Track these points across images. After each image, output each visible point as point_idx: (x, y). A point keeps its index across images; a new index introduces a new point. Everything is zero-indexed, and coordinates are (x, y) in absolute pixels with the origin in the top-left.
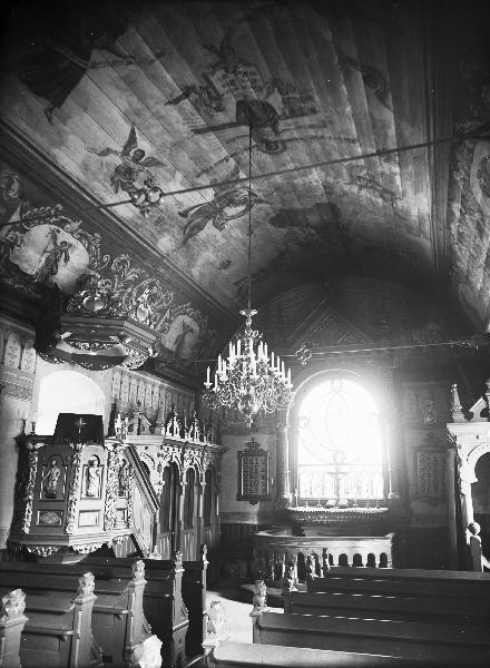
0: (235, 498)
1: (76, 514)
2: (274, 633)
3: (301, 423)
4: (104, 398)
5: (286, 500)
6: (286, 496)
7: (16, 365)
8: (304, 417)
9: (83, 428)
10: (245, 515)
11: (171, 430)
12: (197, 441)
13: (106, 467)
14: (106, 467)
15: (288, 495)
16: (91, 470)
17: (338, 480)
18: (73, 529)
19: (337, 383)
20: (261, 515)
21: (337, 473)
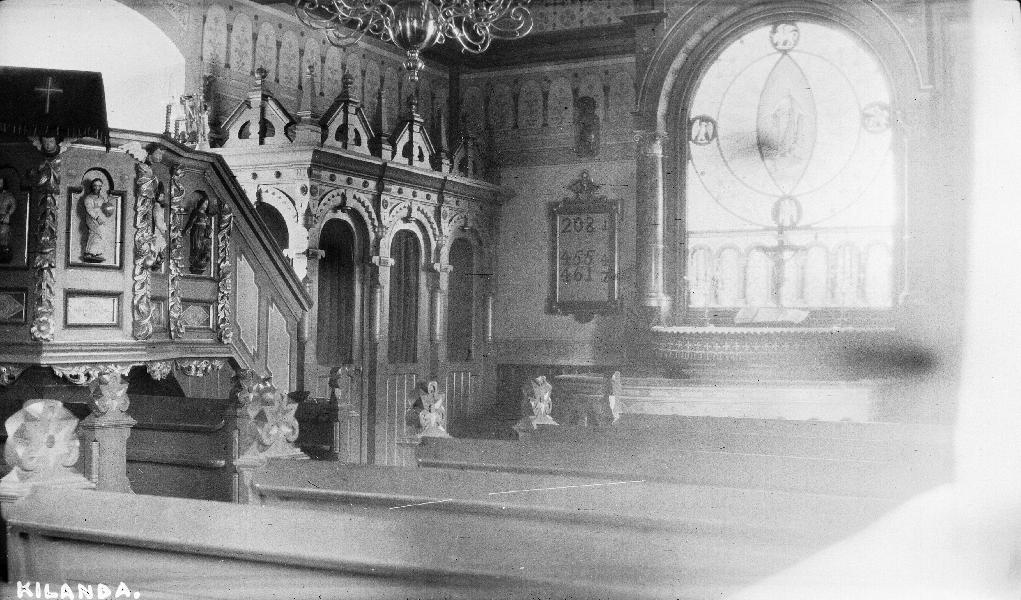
0: (542, 306)
1: (57, 301)
2: (378, 447)
3: (698, 130)
4: (183, 60)
5: (653, 311)
6: (653, 303)
7: (510, 122)
8: (704, 119)
9: (54, 98)
10: (564, 348)
11: (408, 152)
12: (422, 167)
13: (130, 197)
14: (130, 197)
15: (660, 300)
16: (90, 202)
17: (779, 264)
18: (51, 329)
19: (785, 31)
20: (602, 345)
21: (781, 247)
